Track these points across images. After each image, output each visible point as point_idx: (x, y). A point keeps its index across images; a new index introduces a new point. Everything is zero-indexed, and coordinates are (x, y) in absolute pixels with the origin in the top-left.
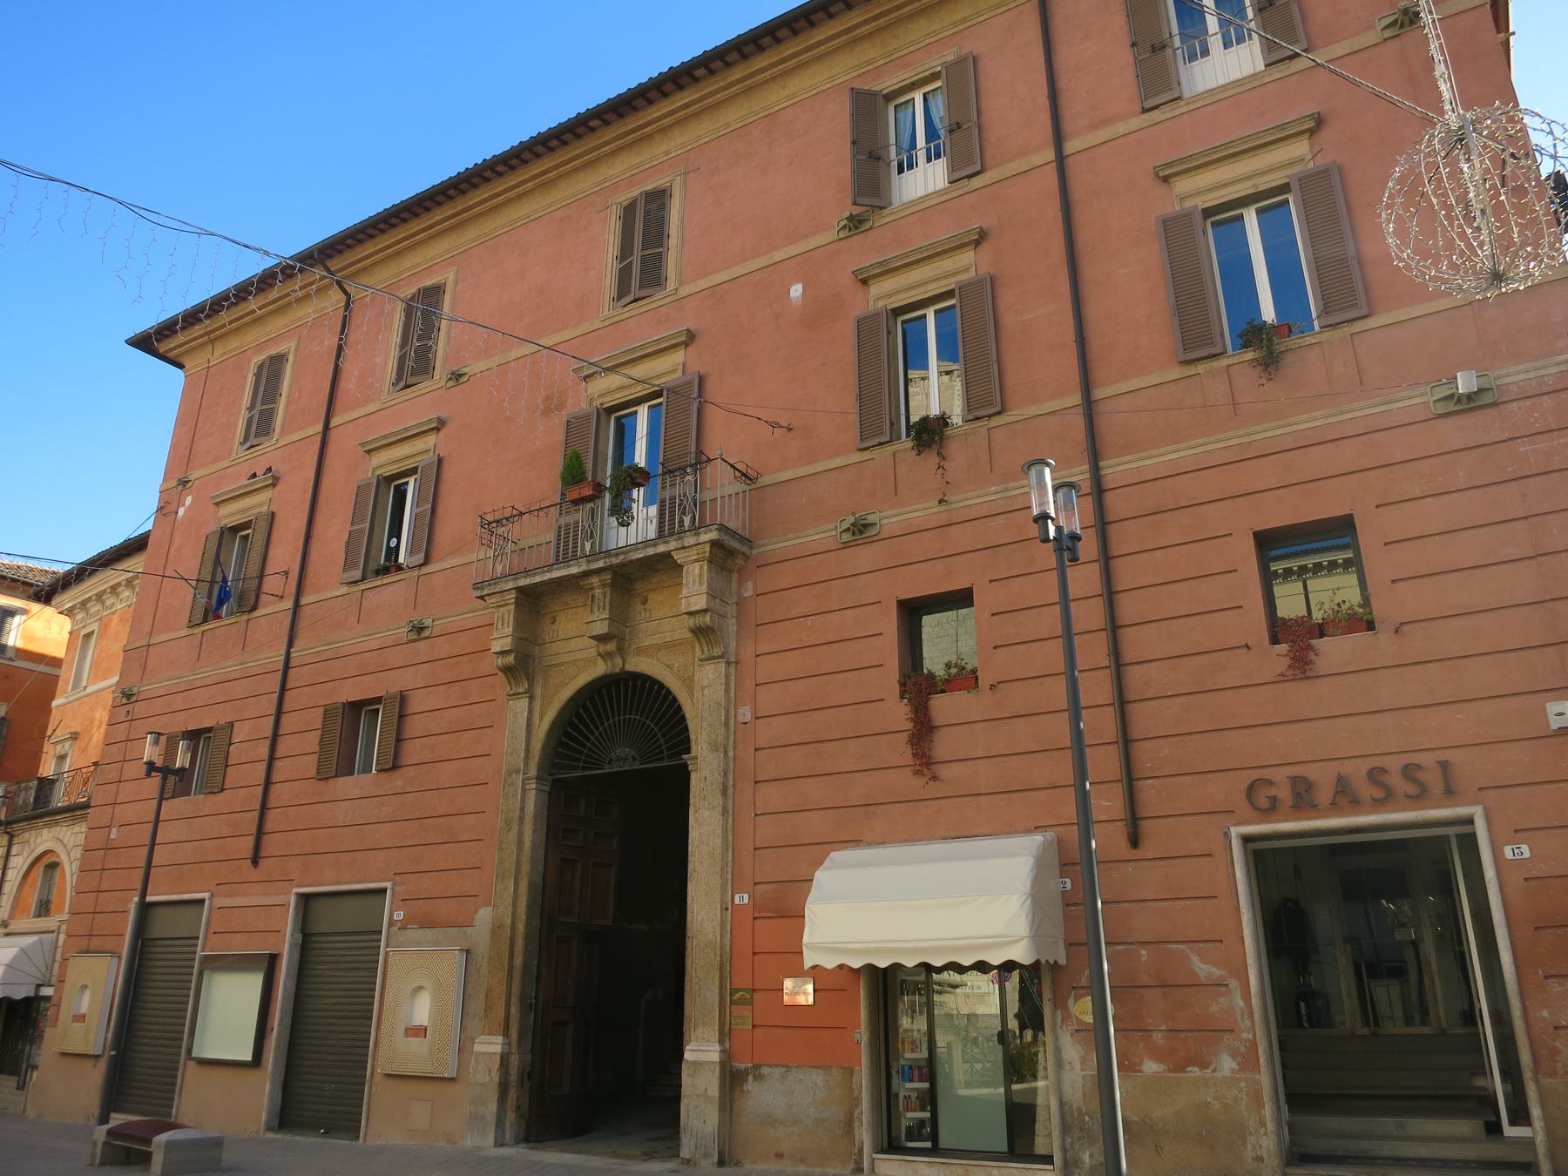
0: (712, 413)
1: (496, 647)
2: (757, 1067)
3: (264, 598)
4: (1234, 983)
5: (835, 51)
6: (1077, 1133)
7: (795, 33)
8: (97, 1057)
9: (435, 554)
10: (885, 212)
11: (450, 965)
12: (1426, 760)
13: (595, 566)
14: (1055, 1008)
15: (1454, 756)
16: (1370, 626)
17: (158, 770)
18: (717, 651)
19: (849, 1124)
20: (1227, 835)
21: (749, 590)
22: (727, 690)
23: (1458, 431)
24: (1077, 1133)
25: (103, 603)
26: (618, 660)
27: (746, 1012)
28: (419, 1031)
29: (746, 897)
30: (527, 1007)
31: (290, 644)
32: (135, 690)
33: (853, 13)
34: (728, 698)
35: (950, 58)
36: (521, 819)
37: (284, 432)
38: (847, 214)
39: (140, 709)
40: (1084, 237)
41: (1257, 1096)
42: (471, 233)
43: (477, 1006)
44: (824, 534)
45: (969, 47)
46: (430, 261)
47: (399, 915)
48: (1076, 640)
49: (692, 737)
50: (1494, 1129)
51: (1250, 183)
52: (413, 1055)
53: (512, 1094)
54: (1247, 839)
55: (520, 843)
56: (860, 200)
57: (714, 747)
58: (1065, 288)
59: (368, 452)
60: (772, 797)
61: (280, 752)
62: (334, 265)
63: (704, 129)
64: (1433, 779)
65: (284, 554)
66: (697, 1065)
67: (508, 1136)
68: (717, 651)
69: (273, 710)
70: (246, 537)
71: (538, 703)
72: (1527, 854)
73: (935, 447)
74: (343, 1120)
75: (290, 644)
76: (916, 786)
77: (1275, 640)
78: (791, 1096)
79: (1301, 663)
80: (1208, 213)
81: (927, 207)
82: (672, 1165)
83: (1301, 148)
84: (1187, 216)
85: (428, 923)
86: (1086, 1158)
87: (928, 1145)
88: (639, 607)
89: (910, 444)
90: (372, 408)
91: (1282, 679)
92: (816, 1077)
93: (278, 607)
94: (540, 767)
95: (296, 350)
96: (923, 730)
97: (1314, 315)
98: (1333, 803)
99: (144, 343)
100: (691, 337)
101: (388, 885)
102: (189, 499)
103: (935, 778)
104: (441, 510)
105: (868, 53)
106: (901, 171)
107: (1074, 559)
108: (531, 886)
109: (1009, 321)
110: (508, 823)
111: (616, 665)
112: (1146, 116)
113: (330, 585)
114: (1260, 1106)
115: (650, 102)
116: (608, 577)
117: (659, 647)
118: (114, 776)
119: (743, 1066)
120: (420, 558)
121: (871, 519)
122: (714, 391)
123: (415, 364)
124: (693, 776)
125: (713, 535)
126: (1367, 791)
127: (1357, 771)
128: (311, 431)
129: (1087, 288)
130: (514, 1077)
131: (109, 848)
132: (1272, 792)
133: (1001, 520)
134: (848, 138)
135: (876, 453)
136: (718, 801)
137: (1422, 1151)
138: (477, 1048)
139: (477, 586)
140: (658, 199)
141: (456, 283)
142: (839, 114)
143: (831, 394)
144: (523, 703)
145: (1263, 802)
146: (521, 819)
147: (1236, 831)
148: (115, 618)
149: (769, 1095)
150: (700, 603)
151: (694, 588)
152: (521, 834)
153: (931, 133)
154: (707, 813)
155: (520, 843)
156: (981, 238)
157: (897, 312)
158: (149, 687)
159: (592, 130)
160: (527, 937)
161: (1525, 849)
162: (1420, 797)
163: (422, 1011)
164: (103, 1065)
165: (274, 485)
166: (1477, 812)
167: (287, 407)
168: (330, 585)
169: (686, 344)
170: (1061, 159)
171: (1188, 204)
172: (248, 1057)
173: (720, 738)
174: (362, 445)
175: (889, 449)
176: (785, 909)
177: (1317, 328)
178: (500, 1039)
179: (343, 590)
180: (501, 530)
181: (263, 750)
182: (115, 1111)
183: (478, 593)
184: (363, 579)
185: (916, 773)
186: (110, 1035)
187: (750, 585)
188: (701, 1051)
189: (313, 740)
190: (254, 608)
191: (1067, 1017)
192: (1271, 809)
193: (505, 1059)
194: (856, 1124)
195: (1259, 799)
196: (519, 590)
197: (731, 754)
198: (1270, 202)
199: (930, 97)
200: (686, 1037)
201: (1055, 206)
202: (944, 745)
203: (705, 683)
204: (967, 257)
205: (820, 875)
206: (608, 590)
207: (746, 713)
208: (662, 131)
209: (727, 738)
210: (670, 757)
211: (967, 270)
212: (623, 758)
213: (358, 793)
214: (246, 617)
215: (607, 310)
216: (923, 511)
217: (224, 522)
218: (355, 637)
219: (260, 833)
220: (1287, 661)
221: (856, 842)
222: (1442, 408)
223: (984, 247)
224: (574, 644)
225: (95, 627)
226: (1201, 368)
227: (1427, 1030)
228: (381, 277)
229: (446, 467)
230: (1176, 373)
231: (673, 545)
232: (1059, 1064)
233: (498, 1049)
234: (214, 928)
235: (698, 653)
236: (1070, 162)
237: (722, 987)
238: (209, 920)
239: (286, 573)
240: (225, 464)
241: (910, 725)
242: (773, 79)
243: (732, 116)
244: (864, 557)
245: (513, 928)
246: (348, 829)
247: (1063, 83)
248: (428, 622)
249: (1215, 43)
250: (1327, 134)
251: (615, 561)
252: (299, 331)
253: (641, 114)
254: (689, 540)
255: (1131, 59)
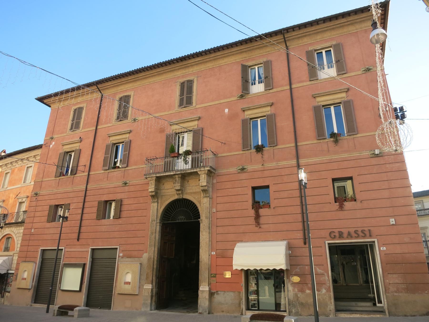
0: (204, 137)
1: (150, 190)
2: (217, 292)
3: (78, 172)
4: (326, 274)
5: (237, 54)
6: (292, 305)
7: (228, 48)
8: (30, 289)
9: (129, 165)
10: (249, 95)
11: (136, 267)
12: (366, 229)
13: (177, 173)
14: (287, 279)
15: (371, 229)
16: (355, 200)
17: (62, 217)
18: (207, 195)
19: (240, 304)
20: (325, 243)
21: (215, 181)
22: (210, 205)
23: (374, 161)
24: (292, 305)
25: (12, 164)
26: (181, 195)
27: (214, 279)
28: (129, 283)
29: (214, 253)
30: (157, 277)
31: (87, 185)
32: (38, 193)
33: (242, 46)
34: (210, 206)
35: (265, 60)
36: (156, 232)
37: (83, 128)
38: (240, 94)
39: (40, 198)
40: (296, 108)
41: (330, 297)
42: (138, 83)
43: (144, 277)
44: (233, 170)
45: (270, 58)
46: (126, 89)
47: (121, 255)
48: (308, 206)
49: (201, 215)
50: (375, 304)
51: (333, 101)
52: (127, 289)
53: (154, 298)
54: (329, 244)
55: (155, 238)
56: (244, 92)
57: (206, 218)
58: (291, 119)
59: (109, 136)
60: (220, 230)
61: (84, 212)
62: (99, 86)
63: (203, 67)
64: (367, 233)
65: (84, 160)
66: (203, 291)
67: (153, 308)
68: (207, 195)
69: (83, 201)
70: (70, 154)
71: (159, 204)
72: (385, 249)
73: (261, 152)
74: (106, 304)
75: (87, 185)
76: (257, 229)
77: (336, 202)
78: (225, 298)
79: (341, 207)
80: (323, 106)
81: (258, 96)
82: (196, 314)
83: (344, 95)
84: (319, 107)
85: (129, 257)
86: (294, 311)
87: (257, 309)
88: (186, 183)
89: (255, 150)
90: (109, 125)
91: (337, 210)
92: (232, 294)
93: (82, 174)
94: (160, 220)
95: (86, 107)
96: (257, 217)
97: (346, 133)
98: (347, 237)
99: (41, 100)
100: (199, 118)
101: (118, 247)
102: (53, 143)
103: (260, 228)
104: (131, 154)
105: (244, 55)
106: (252, 85)
107: (306, 188)
108: (158, 248)
109: (278, 124)
110: (152, 233)
111: (181, 197)
112: (310, 82)
113: (98, 170)
114: (331, 299)
115: (190, 59)
116: (180, 176)
117: (192, 193)
118: (32, 215)
119: (214, 291)
120: (125, 165)
121: (245, 167)
122: (206, 133)
123: (122, 115)
124: (201, 224)
125: (209, 168)
126: (354, 235)
127: (352, 231)
128: (91, 129)
129: (296, 120)
130: (154, 294)
131: (31, 234)
132: (334, 234)
133: (276, 170)
134: (241, 77)
135: (247, 152)
136: (208, 230)
137: (361, 309)
138: (144, 287)
139: (145, 175)
140: (190, 82)
141: (134, 95)
142: (238, 70)
143: (236, 137)
144: (156, 204)
145: (332, 236)
146: (156, 232)
147: (327, 242)
148: (16, 170)
149: (219, 298)
150: (205, 184)
151: (203, 180)
152: (155, 236)
153: (260, 77)
154: (205, 233)
155: (155, 238)
156: (272, 105)
157: (251, 119)
158: (43, 192)
159: (174, 63)
160: (157, 261)
161: (385, 248)
162: (365, 236)
163: (129, 278)
164: (32, 291)
165: (80, 142)
166: (376, 240)
167: (84, 122)
168: (98, 170)
169: (198, 120)
170: (291, 89)
171: (319, 104)
172: (78, 289)
173: (208, 216)
174: (108, 135)
175: (249, 151)
176: (226, 257)
177: (346, 135)
178: (151, 285)
179: (103, 171)
180: (151, 162)
181: (80, 211)
182: (256, 290)
183: (145, 177)
184: (109, 169)
185: (256, 226)
186: (34, 284)
187: (215, 180)
188: (204, 288)
189: (95, 210)
190: (76, 174)
191: (290, 281)
192: (334, 238)
193: (152, 290)
194: (241, 304)
195: (332, 235)
196: (157, 177)
197: (211, 219)
198: (337, 105)
199: (259, 68)
200: (199, 285)
201: (289, 100)
202: (262, 220)
203: (204, 202)
204: (268, 108)
205: (235, 249)
206: (180, 179)
207: (214, 210)
208: (192, 66)
209: (210, 216)
210: (194, 219)
211: (268, 111)
212: (181, 219)
213: (108, 224)
214: (73, 176)
215: (176, 109)
216: (258, 167)
217: (65, 150)
218: (107, 184)
219: (79, 233)
220: (338, 207)
221: (241, 241)
222: (372, 156)
223: (273, 106)
224: (169, 191)
225: (10, 171)
226: (321, 141)
227: (358, 284)
228: (112, 91)
229: (132, 143)
230: (316, 141)
231: (198, 170)
232: (288, 291)
233: (151, 287)
234: (65, 256)
235: (202, 195)
236: (293, 90)
237: (209, 273)
238: (64, 254)
239: (85, 166)
240: (65, 135)
241: (255, 215)
242: (221, 58)
243: (210, 65)
244: (243, 176)
245: (154, 258)
246: (105, 233)
247: (292, 71)
248: (128, 182)
249: (326, 67)
250: (350, 93)
251: (183, 172)
252: (88, 102)
253: (187, 61)
254: (202, 169)
255: (307, 68)
